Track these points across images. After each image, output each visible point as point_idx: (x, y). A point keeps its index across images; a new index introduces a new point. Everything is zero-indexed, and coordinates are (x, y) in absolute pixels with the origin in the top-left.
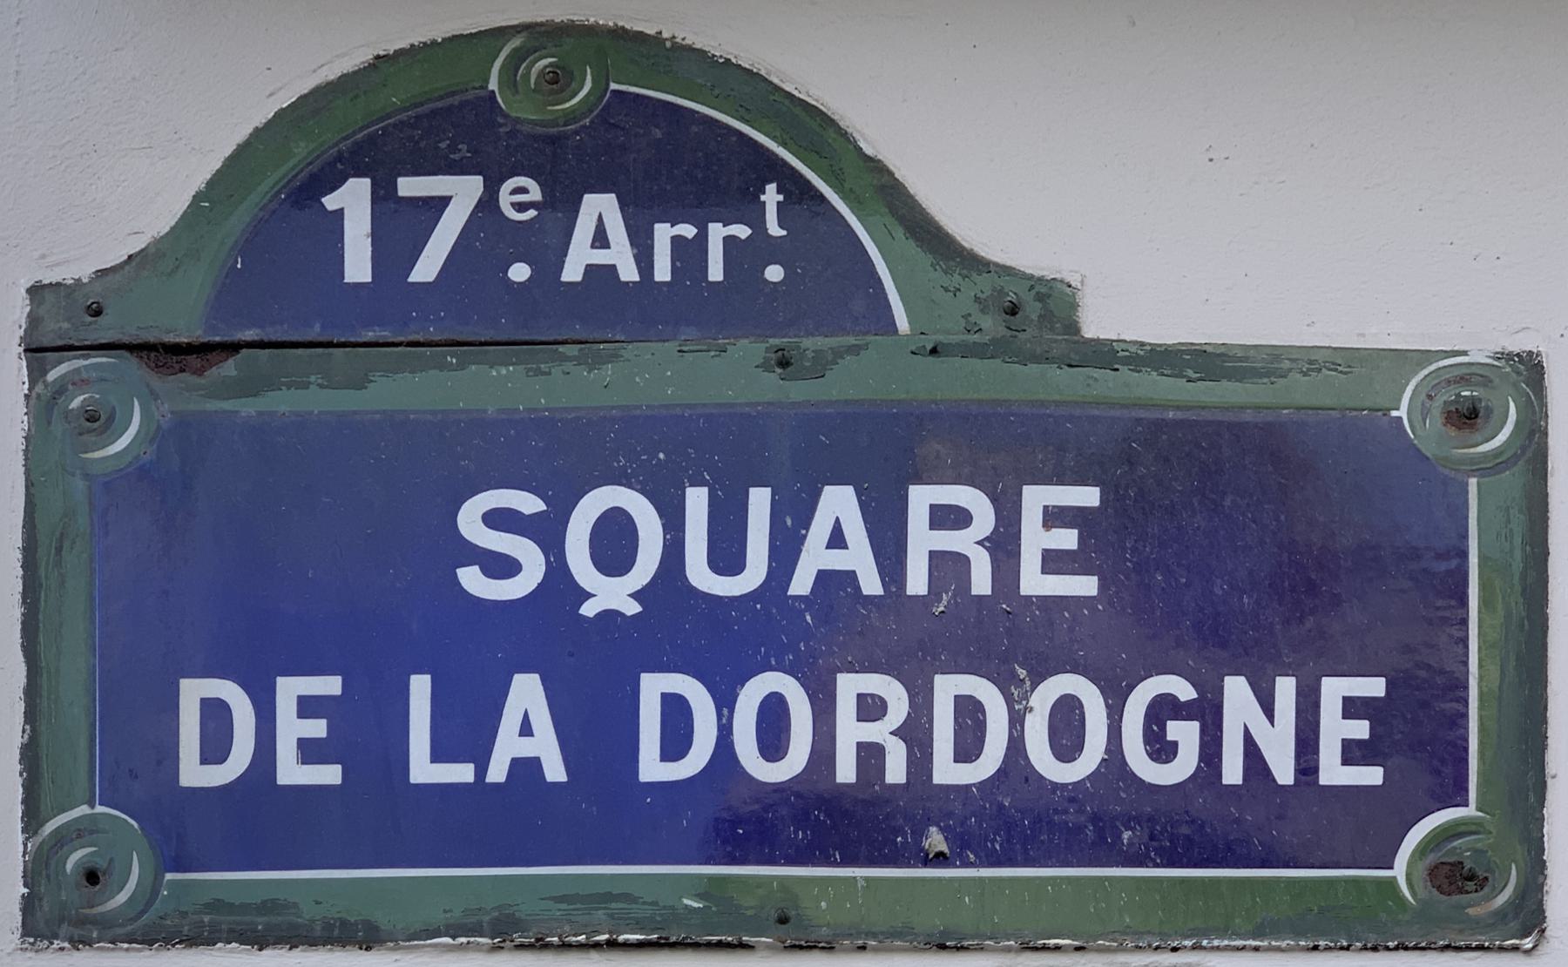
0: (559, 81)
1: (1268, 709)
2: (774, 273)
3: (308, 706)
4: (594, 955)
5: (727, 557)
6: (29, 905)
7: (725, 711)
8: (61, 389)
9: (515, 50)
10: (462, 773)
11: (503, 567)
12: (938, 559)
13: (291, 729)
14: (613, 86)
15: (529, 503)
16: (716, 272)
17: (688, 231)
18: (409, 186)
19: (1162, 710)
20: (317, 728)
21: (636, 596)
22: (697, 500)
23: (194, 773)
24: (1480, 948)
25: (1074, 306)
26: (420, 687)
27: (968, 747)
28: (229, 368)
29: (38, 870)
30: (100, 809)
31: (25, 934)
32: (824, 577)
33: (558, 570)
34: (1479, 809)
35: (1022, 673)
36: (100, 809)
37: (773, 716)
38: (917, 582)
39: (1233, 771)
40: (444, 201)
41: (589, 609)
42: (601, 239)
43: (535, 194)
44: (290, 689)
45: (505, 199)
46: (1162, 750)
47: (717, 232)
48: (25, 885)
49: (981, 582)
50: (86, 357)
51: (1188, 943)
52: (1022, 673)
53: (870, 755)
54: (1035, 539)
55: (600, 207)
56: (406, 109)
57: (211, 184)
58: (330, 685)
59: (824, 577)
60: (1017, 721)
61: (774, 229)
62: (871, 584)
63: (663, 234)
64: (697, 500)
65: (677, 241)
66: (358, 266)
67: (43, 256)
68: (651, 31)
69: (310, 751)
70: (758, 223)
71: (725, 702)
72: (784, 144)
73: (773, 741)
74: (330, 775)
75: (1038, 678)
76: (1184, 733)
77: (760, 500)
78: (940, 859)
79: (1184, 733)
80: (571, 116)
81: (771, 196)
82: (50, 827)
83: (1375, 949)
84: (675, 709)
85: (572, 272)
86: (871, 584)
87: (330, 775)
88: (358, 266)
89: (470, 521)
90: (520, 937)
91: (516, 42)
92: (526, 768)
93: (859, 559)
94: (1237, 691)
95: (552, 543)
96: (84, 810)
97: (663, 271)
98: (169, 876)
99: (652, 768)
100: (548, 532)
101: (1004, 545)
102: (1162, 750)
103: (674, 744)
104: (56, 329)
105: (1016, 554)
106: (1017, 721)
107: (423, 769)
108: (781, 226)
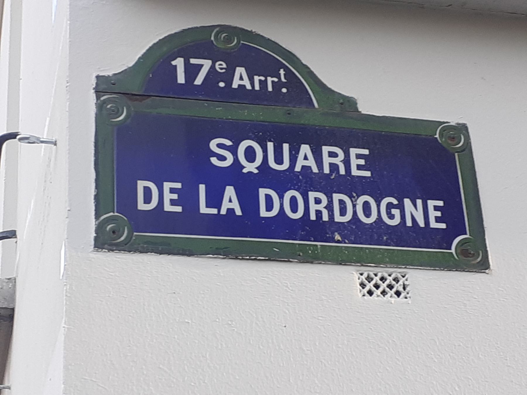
0: (229, 40)
1: (415, 206)
2: (284, 90)
3: (172, 191)
4: (250, 261)
5: (279, 160)
6: (96, 239)
7: (281, 199)
8: (104, 102)
9: (217, 31)
10: (214, 211)
11: (222, 158)
12: (331, 164)
13: (168, 196)
14: (242, 42)
15: (228, 143)
16: (270, 89)
17: (263, 78)
18: (193, 61)
19: (390, 206)
20: (175, 196)
21: (257, 168)
22: (270, 146)
23: (142, 206)
24: (475, 272)
25: (356, 104)
26: (202, 188)
27: (343, 212)
28: (149, 101)
29: (99, 229)
30: (116, 214)
31: (95, 247)
32: (303, 167)
33: (236, 160)
34: (470, 235)
35: (355, 195)
36: (116, 214)
37: (293, 201)
38: (327, 170)
39: (409, 223)
40: (201, 66)
41: (245, 171)
42: (241, 78)
43: (224, 66)
44: (167, 186)
45: (217, 67)
46: (391, 217)
47: (270, 79)
48: (96, 233)
49: (342, 171)
50: (111, 95)
51: (403, 267)
52: (355, 195)
53: (319, 213)
54: (354, 162)
55: (240, 71)
56: (191, 42)
57: (143, 55)
58: (178, 185)
59: (303, 167)
60: (354, 206)
61: (283, 79)
62: (315, 170)
63: (257, 78)
64: (270, 146)
65: (260, 81)
66: (181, 79)
67: (99, 68)
68: (249, 30)
69: (173, 202)
70: (279, 78)
71: (281, 197)
72: (284, 60)
73: (294, 208)
74: (179, 209)
75: (358, 196)
76: (396, 212)
77: (286, 147)
78: (338, 242)
79: (396, 212)
80: (232, 48)
81: (282, 72)
82: (102, 218)
83: (450, 270)
84: (269, 198)
85: (235, 85)
86: (315, 170)
87: (179, 209)
88: (181, 79)
89: (213, 145)
90: (231, 256)
91: (217, 29)
92: (231, 211)
93: (311, 163)
94: (407, 202)
95: (235, 153)
96: (112, 214)
97: (257, 87)
98: (135, 234)
99: (263, 213)
100: (233, 150)
101: (347, 162)
102: (391, 217)
103: (269, 207)
104: (102, 87)
105: (350, 166)
106: (354, 206)
107: (204, 209)
108: (285, 78)
